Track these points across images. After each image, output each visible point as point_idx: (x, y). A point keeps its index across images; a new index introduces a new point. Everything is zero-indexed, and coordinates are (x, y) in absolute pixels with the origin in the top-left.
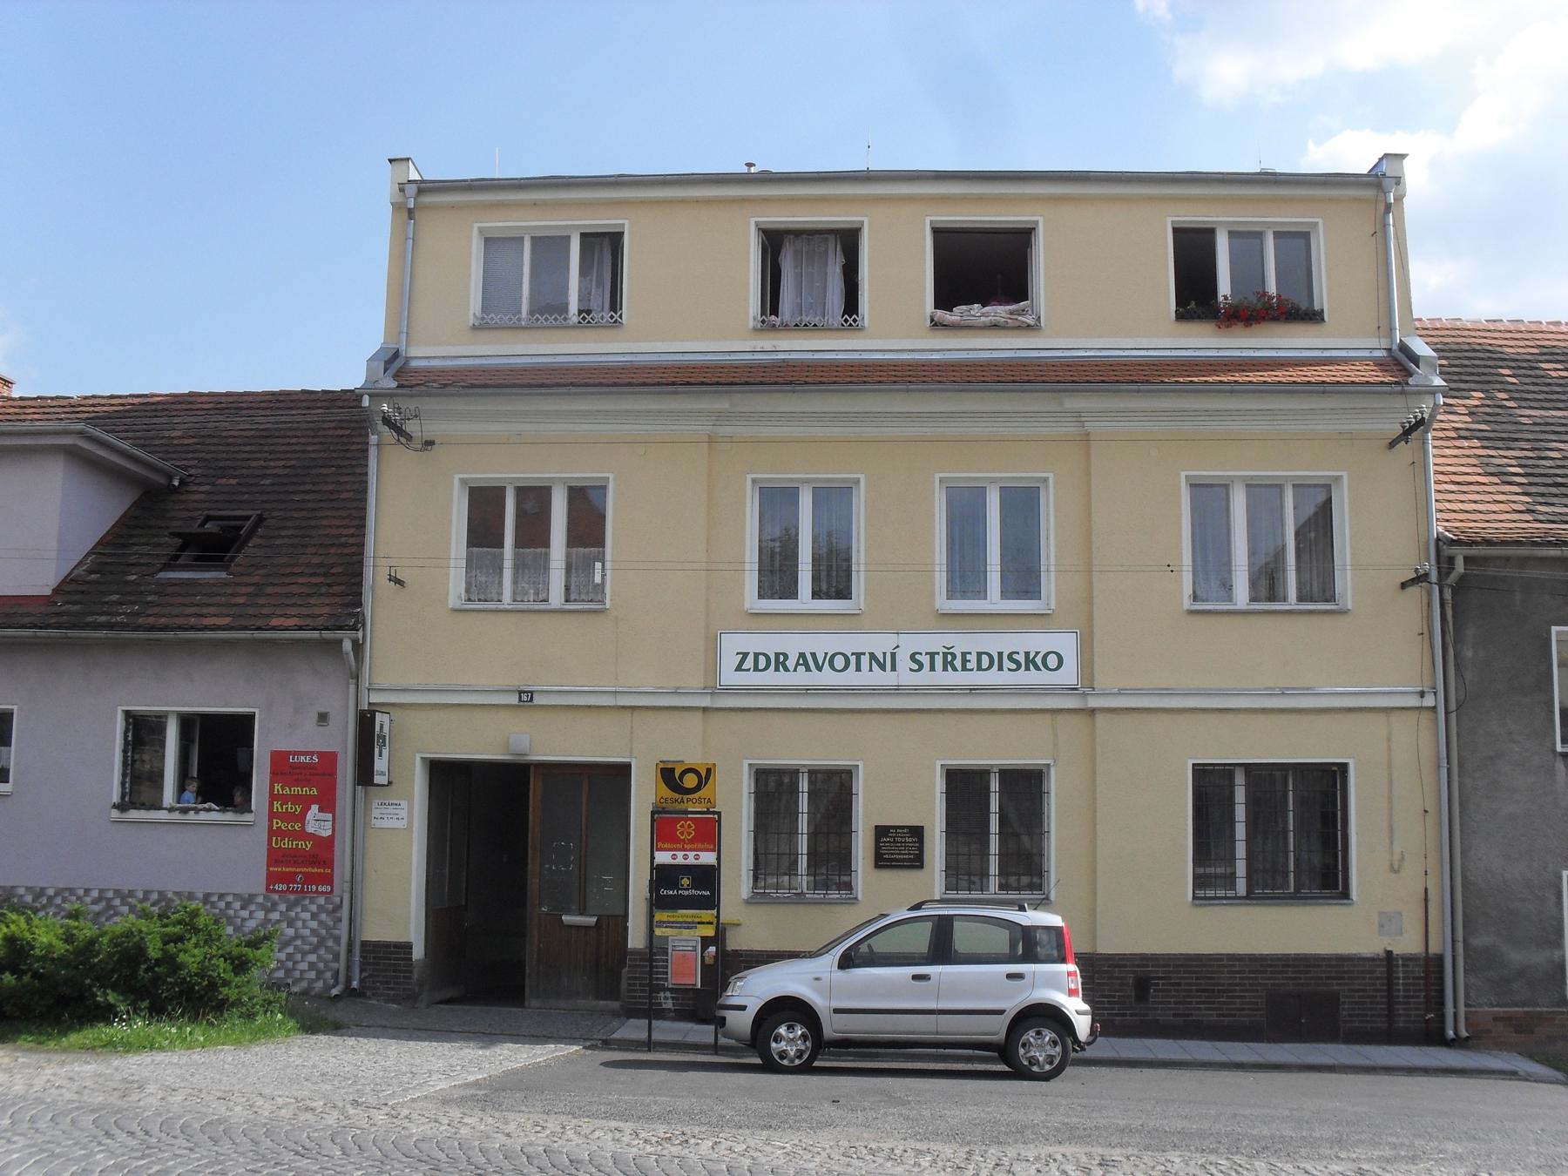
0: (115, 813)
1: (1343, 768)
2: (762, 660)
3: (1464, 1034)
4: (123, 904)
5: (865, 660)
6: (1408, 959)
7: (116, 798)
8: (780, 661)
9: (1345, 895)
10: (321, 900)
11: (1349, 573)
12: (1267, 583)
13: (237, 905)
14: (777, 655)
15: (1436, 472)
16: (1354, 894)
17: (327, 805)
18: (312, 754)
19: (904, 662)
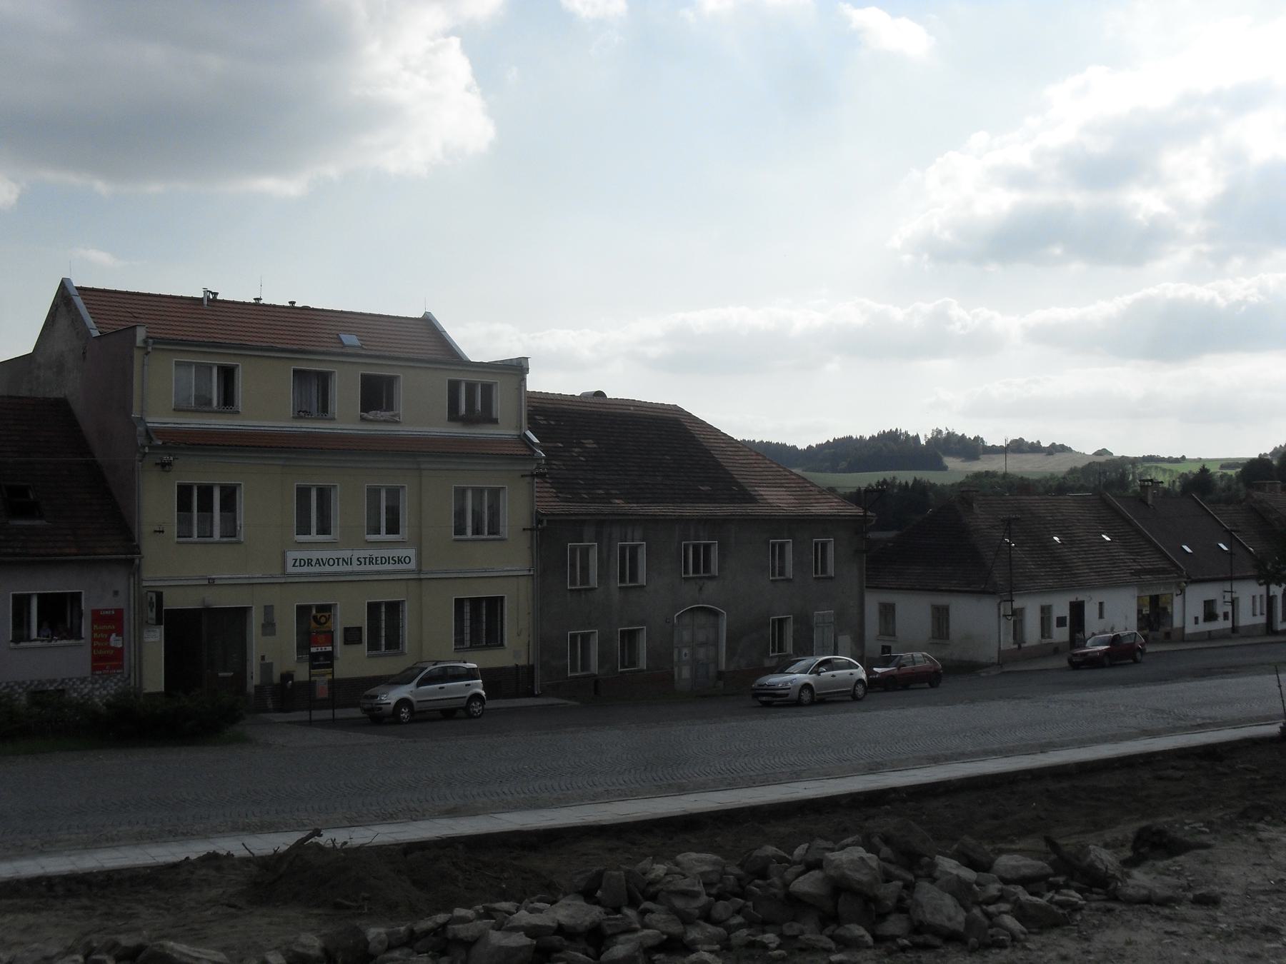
0: (12, 645)
1: (502, 598)
2: (302, 561)
3: (540, 692)
4: (19, 688)
5: (341, 560)
6: (523, 667)
7: (11, 639)
8: (309, 562)
9: (502, 644)
10: (119, 676)
11: (507, 528)
12: (477, 530)
13: (78, 683)
14: (308, 560)
15: (537, 487)
16: (506, 643)
17: (120, 632)
18: (111, 610)
19: (355, 562)
